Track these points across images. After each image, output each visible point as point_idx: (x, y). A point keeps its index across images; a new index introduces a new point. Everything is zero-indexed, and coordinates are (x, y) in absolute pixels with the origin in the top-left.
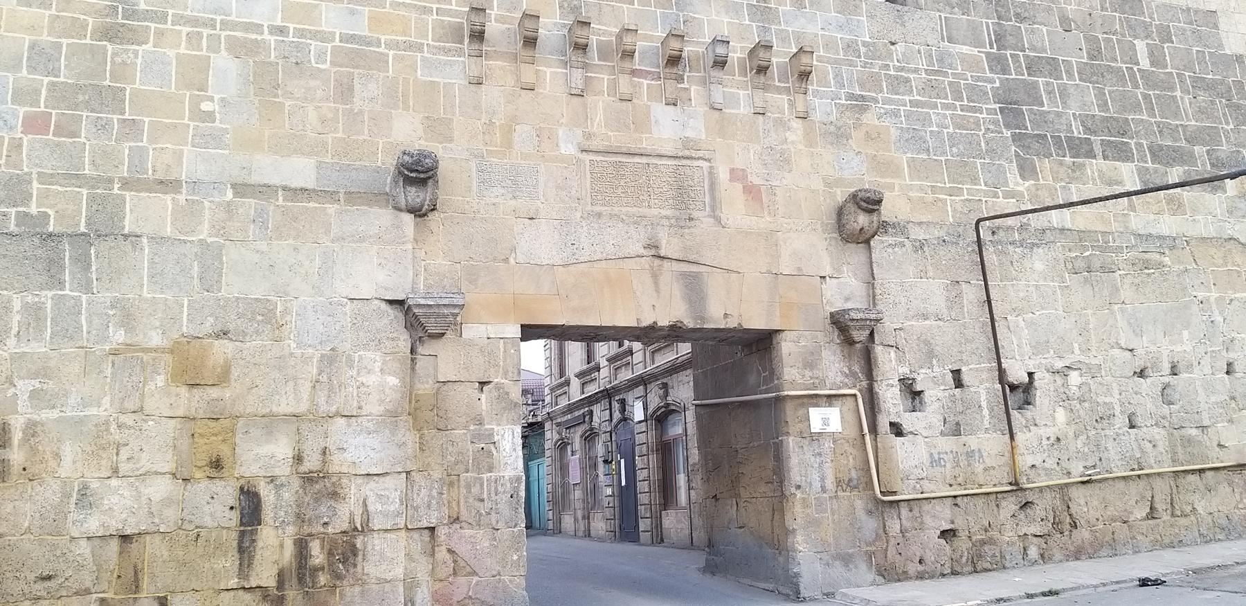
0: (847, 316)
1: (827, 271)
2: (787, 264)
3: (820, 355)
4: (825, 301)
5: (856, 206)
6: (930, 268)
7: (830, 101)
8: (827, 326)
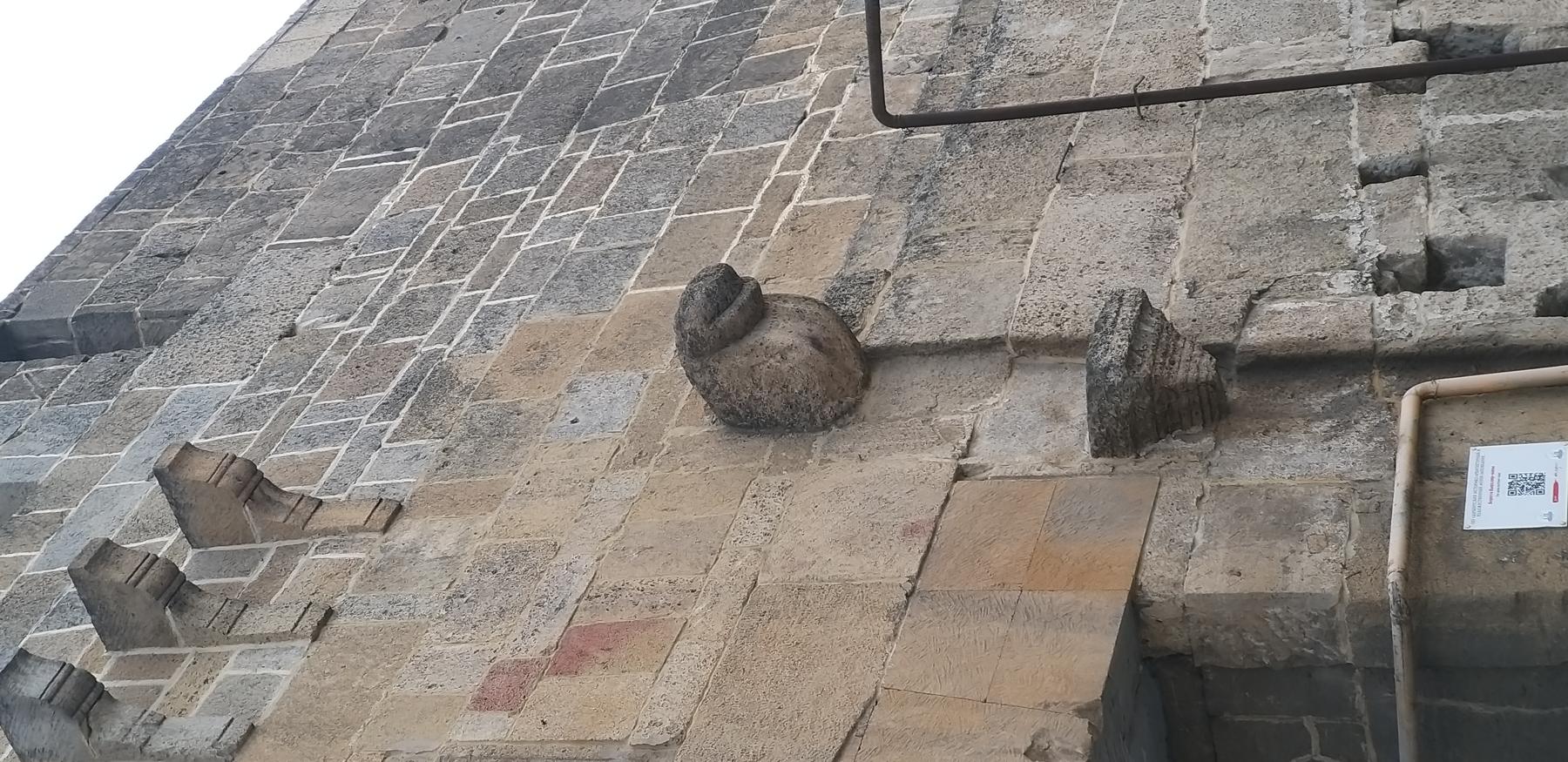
0: (1114, 377)
1: (941, 460)
2: (881, 562)
3: (1252, 491)
4: (1048, 470)
5: (731, 348)
6: (1001, 224)
7: (375, 455)
8: (1145, 465)
